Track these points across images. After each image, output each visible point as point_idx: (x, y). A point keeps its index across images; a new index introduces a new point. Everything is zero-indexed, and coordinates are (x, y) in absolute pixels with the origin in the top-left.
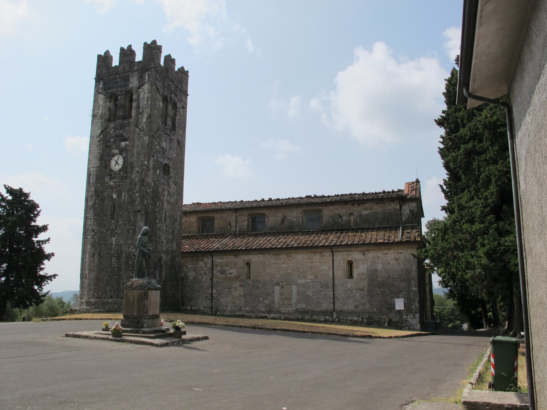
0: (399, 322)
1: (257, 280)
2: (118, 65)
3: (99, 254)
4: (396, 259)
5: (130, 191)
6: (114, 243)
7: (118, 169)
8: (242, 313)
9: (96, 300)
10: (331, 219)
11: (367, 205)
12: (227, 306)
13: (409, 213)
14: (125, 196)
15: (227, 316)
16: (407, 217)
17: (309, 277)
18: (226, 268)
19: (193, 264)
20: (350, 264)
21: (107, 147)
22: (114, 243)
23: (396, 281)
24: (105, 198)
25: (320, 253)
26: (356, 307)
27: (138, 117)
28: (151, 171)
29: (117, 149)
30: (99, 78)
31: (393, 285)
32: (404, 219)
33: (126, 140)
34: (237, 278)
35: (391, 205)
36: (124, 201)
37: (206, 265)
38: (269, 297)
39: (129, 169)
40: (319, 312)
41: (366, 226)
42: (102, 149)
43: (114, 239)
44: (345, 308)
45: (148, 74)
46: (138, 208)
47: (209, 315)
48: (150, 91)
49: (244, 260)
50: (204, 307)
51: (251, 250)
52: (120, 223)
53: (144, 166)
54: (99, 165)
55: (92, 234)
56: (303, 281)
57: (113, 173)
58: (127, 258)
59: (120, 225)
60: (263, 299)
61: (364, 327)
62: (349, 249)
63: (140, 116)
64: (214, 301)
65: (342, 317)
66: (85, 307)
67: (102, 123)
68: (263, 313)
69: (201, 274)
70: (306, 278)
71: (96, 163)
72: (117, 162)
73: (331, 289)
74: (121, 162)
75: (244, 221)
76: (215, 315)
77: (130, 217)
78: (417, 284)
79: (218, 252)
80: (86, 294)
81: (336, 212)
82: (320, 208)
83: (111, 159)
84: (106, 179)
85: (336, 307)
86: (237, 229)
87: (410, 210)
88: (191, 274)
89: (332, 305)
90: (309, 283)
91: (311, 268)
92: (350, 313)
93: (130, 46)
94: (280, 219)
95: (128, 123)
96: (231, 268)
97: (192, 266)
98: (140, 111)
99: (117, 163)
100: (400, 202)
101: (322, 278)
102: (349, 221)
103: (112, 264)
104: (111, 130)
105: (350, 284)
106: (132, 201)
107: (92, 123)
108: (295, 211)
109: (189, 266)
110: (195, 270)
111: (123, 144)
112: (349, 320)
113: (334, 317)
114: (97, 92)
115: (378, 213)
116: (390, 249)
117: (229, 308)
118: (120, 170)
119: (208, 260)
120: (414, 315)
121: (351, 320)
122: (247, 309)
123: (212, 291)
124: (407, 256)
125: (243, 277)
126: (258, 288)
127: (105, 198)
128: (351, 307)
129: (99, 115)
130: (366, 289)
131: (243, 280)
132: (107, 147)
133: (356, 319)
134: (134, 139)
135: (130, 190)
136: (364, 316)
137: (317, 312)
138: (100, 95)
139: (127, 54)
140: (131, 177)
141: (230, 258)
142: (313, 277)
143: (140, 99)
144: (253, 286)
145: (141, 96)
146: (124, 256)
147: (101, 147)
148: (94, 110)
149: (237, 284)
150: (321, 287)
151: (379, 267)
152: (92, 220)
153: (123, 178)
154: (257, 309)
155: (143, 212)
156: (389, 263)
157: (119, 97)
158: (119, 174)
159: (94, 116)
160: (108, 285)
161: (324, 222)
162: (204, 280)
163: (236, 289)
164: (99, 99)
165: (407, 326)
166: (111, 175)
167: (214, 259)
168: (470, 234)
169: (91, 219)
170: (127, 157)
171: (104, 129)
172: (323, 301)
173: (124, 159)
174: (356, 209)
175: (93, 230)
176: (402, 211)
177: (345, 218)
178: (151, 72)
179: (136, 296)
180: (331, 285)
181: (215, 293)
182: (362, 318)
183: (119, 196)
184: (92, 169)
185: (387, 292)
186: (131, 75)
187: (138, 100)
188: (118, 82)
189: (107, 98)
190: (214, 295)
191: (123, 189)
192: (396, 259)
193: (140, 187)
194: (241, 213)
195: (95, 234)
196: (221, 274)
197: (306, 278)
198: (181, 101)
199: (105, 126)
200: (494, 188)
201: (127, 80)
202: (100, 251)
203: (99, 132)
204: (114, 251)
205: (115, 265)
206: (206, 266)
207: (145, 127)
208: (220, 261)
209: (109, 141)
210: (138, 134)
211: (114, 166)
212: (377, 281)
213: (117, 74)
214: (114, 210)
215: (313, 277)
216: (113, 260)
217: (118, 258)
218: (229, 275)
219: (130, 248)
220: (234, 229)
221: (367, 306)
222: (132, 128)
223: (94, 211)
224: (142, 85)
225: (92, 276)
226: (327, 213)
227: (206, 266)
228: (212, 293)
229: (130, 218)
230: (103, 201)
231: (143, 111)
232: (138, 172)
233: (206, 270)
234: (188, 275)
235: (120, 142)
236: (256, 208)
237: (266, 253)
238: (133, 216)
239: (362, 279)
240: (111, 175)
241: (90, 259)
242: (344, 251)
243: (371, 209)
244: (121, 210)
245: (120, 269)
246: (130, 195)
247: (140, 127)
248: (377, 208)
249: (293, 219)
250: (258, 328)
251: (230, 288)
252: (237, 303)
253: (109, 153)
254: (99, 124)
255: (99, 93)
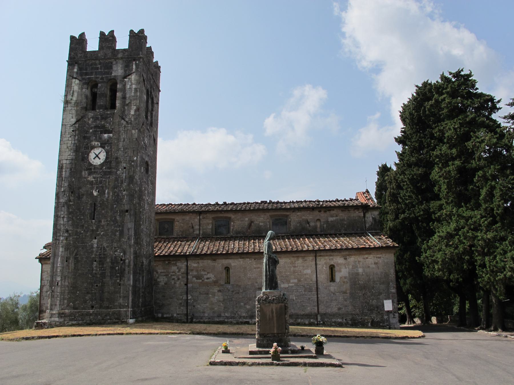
0: (380, 322)
1: (237, 285)
2: (97, 49)
3: (76, 258)
4: (376, 263)
5: (114, 188)
6: (95, 246)
7: (99, 163)
8: (221, 319)
9: (72, 311)
10: (298, 225)
11: (332, 212)
12: (204, 312)
13: (371, 220)
14: (108, 194)
15: (204, 323)
16: (370, 224)
17: (291, 281)
18: (203, 273)
19: (164, 269)
20: (332, 268)
21: (85, 138)
22: (95, 246)
23: (376, 284)
24: (83, 195)
25: (303, 257)
26: (339, 309)
27: (124, 108)
28: (139, 168)
29: (98, 141)
30: (72, 62)
31: (373, 287)
32: (367, 226)
33: (109, 132)
34: (215, 283)
35: (355, 212)
36: (107, 199)
37: (179, 269)
38: (251, 302)
39: (113, 164)
40: (303, 315)
41: (333, 232)
42: (78, 140)
43: (95, 241)
44: (329, 311)
45: (136, 64)
46: (126, 207)
47: (184, 322)
48: (138, 83)
49: (223, 265)
50: (178, 314)
51: (232, 254)
52: (103, 223)
53: (133, 161)
54: (74, 157)
55: (66, 235)
56: (286, 285)
57: (93, 168)
58: (112, 263)
59: (103, 226)
60: (245, 304)
61: (350, 328)
62: (332, 254)
63: (126, 108)
64: (189, 308)
65: (326, 320)
66: (57, 319)
67: (77, 111)
68: (244, 318)
69: (174, 279)
70: (288, 282)
71: (69, 155)
72: (97, 156)
73: (315, 293)
74: (103, 156)
75: (208, 225)
76: (191, 322)
77: (115, 217)
78: (395, 286)
79: (194, 256)
80: (58, 303)
81: (303, 217)
82: (288, 213)
83: (90, 152)
84: (83, 173)
85: (320, 310)
86: (201, 232)
87: (373, 218)
88: (162, 280)
89: (316, 308)
90: (292, 287)
91: (294, 272)
92: (334, 315)
93: (112, 32)
94: (247, 223)
95: (111, 114)
96: (208, 273)
97: (163, 271)
98: (127, 103)
99: (97, 157)
100: (363, 211)
101: (306, 282)
102: (316, 227)
103: (93, 270)
104: (89, 119)
105: (333, 287)
106: (118, 199)
107: (64, 111)
108: (262, 216)
109: (159, 271)
110: (166, 275)
111: (106, 135)
112: (333, 322)
113: (319, 320)
114: (70, 76)
115: (343, 220)
116: (370, 254)
117: (206, 315)
118: (102, 165)
119: (182, 265)
120: (394, 315)
121: (335, 322)
122: (226, 315)
123: (187, 297)
124: (386, 261)
125: (222, 282)
126: (238, 293)
127: (83, 195)
128: (335, 310)
129: (73, 102)
130: (348, 292)
131: (222, 285)
132: (85, 138)
133: (340, 320)
134: (119, 131)
135: (115, 187)
136: (348, 318)
137: (301, 315)
138: (74, 80)
139: (107, 40)
140: (116, 173)
141: (208, 262)
142: (296, 281)
143: (111, 90)
144: (233, 291)
145: (128, 87)
146: (108, 260)
147: (76, 137)
148: (66, 96)
149: (216, 289)
150: (305, 291)
151: (360, 270)
152: (65, 219)
153: (105, 173)
154: (238, 314)
155: (132, 212)
156: (369, 267)
157: (99, 85)
158: (101, 169)
159: (66, 102)
160: (88, 293)
161: (292, 227)
162: (177, 285)
163: (214, 295)
164: (73, 84)
165: (387, 325)
166: (91, 169)
167: (189, 263)
168: (485, 241)
169: (63, 218)
170: (111, 151)
171: (80, 117)
172: (307, 304)
173: (107, 153)
174: (323, 216)
175: (67, 231)
176: (366, 219)
177: (312, 224)
178: (140, 62)
179: (274, 310)
180: (314, 288)
181: (191, 299)
182: (346, 320)
183: (101, 193)
184: (64, 162)
185: (369, 294)
186: (114, 62)
187: (124, 90)
188: (98, 68)
189: (84, 84)
190: (189, 301)
191: (106, 186)
192: (376, 263)
193: (129, 185)
194: (205, 216)
195: (70, 235)
196: (197, 279)
197: (288, 282)
198: (156, 96)
199: (82, 115)
200: (499, 201)
201: (109, 67)
202: (76, 254)
203: (74, 120)
204: (96, 255)
205: (96, 270)
206: (179, 271)
207: (133, 120)
208: (195, 265)
209: (87, 132)
210: (125, 127)
211: (92, 159)
212: (359, 284)
213: (97, 59)
214: (95, 209)
215: (296, 281)
216: (95, 265)
217: (101, 262)
218: (206, 280)
219: (116, 251)
220: (198, 232)
221: (350, 308)
222: (117, 119)
223: (68, 208)
224: (129, 75)
225: (67, 284)
226: (294, 219)
227: (179, 271)
228: (187, 299)
229: (116, 219)
230: (79, 197)
231: (130, 103)
232: (125, 168)
233: (179, 275)
234: (158, 280)
235: (101, 133)
236: (218, 211)
237: (247, 258)
238: (120, 215)
239: (344, 282)
240: (91, 169)
241: (62, 263)
242: (327, 256)
243: (337, 216)
244: (104, 209)
245: (103, 275)
246: (115, 193)
247: (127, 120)
248: (343, 215)
249: (261, 224)
250: (299, 336)
251: (208, 294)
252: (216, 309)
253: (87, 144)
254: (74, 112)
255: (73, 78)
